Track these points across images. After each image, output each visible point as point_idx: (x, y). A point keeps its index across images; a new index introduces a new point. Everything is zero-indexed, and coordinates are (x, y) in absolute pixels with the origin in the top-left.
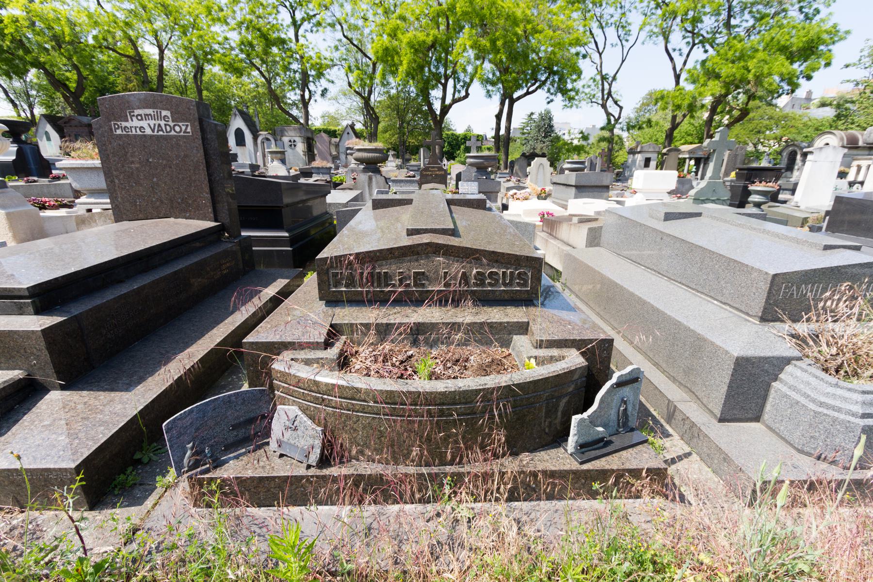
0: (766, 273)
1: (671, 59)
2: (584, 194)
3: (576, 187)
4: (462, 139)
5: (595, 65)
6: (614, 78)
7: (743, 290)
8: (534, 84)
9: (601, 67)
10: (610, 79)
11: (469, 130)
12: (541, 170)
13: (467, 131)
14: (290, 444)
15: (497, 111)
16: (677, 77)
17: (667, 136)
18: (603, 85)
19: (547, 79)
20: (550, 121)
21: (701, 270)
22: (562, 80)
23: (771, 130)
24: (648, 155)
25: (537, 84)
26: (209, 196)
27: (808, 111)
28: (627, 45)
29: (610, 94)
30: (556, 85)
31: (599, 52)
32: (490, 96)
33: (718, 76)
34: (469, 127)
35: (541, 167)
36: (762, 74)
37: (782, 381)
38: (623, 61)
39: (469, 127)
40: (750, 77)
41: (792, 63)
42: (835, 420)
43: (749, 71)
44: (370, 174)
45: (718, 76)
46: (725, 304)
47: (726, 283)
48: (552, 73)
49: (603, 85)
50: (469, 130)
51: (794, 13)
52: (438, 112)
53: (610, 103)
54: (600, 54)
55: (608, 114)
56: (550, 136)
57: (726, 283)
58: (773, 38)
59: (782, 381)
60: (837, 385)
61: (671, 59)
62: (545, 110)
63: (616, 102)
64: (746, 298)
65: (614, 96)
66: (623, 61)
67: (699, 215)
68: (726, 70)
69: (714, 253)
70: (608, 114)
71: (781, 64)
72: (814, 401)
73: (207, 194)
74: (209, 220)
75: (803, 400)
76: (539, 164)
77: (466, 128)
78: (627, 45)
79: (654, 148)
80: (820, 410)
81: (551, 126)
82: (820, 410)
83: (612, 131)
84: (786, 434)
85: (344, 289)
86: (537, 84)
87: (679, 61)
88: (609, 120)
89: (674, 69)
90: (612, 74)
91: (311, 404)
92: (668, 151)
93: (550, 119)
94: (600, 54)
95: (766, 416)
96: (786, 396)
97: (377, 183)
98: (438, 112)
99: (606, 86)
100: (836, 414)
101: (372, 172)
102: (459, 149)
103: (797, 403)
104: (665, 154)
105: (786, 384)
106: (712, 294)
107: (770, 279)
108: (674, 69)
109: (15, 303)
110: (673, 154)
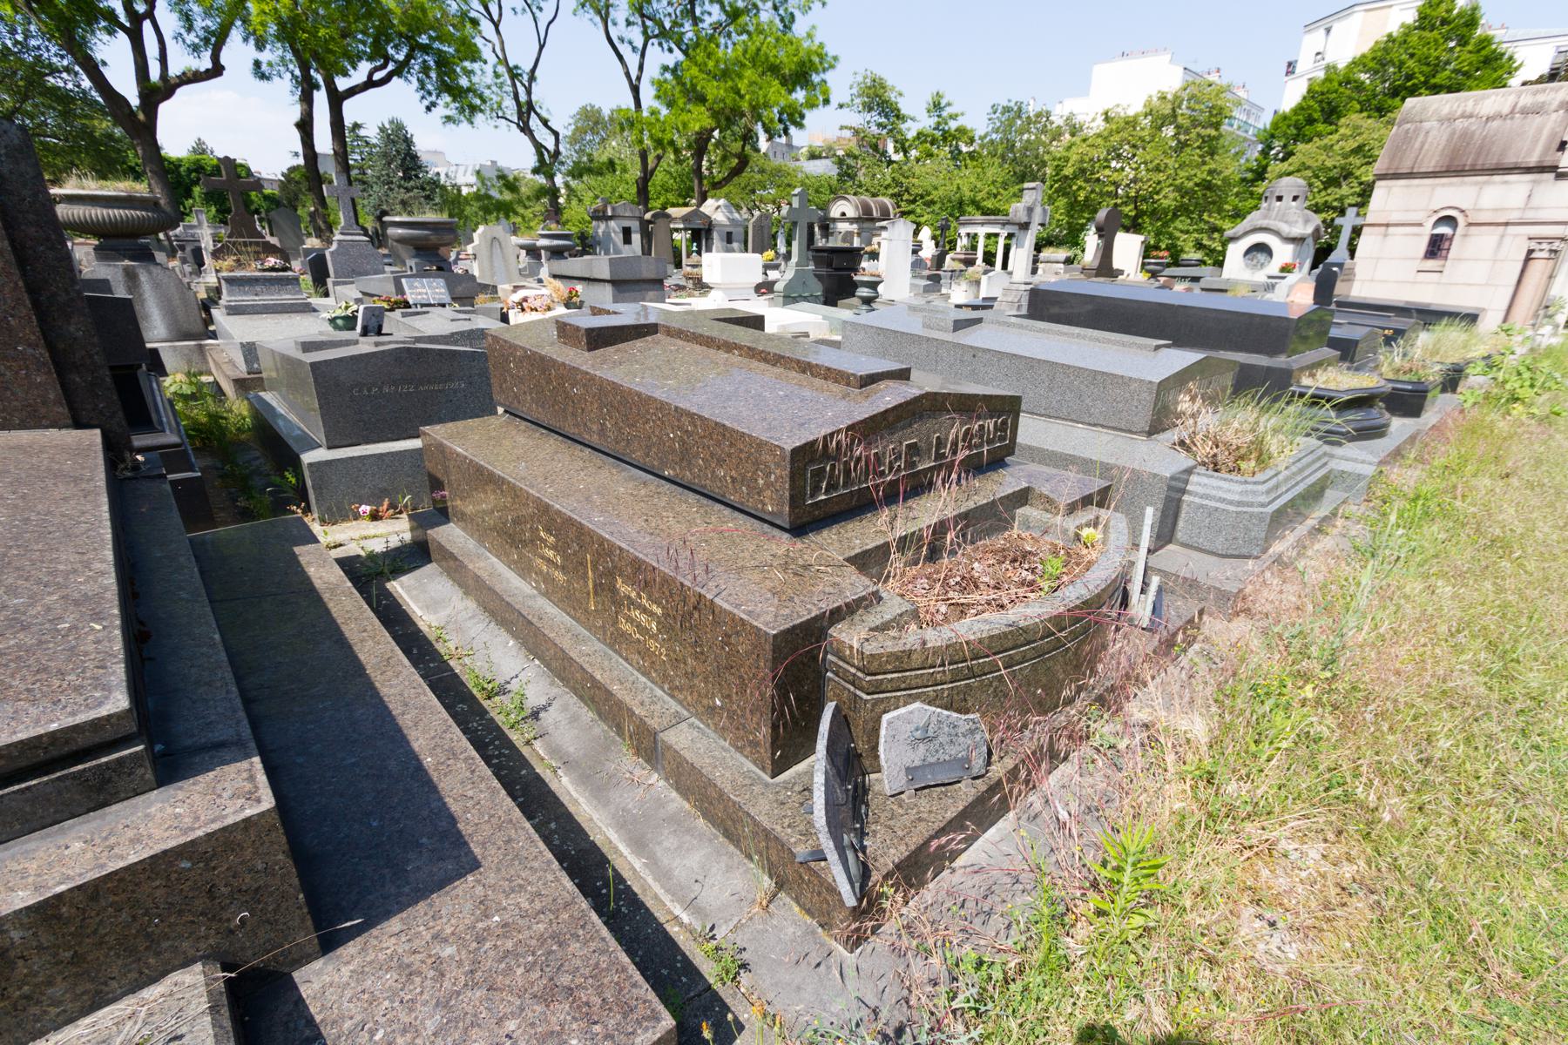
0: (1150, 382)
1: (620, 58)
2: (627, 295)
3: (613, 282)
4: (189, 171)
5: (490, 45)
6: (532, 78)
7: (1120, 405)
8: (384, 67)
9: (503, 50)
10: (526, 77)
11: (200, 148)
12: (497, 250)
13: (194, 151)
14: (931, 764)
15: (296, 113)
16: (635, 90)
17: (639, 192)
18: (514, 85)
19: (409, 57)
20: (409, 146)
21: (1051, 390)
22: (443, 63)
23: (764, 188)
24: (627, 223)
25: (391, 67)
26: (42, 353)
27: (798, 163)
28: (543, 19)
29: (531, 106)
30: (433, 75)
31: (492, 20)
32: (263, 77)
33: (702, 99)
34: (200, 142)
35: (496, 244)
36: (758, 104)
37: (1190, 493)
38: (542, 47)
39: (200, 142)
40: (745, 106)
41: (790, 92)
42: (1252, 515)
43: (742, 97)
44: (127, 262)
45: (702, 99)
46: (1095, 425)
47: (1093, 400)
48: (415, 48)
49: (514, 85)
50: (200, 148)
51: (766, 15)
52: (134, 101)
53: (534, 122)
54: (496, 25)
55: (539, 147)
56: (417, 176)
57: (1093, 400)
58: (759, 50)
59: (1190, 493)
60: (1246, 482)
61: (620, 58)
62: (391, 122)
63: (545, 123)
64: (1125, 413)
65: (538, 110)
66: (542, 47)
67: (979, 321)
68: (715, 91)
69: (1069, 367)
70: (539, 147)
71: (774, 89)
72: (1231, 503)
73: (34, 346)
74: (55, 424)
75: (1218, 505)
76: (489, 238)
77: (192, 143)
78: (543, 19)
79: (631, 210)
80: (1240, 509)
81: (415, 157)
82: (1240, 509)
83: (551, 177)
84: (1207, 546)
85: (823, 497)
86: (391, 67)
87: (632, 60)
88: (540, 155)
89: (628, 75)
90: (526, 66)
91: (899, 694)
92: (653, 216)
93: (408, 142)
94: (496, 25)
95: (1179, 535)
96: (1202, 506)
97: (157, 286)
98: (134, 101)
99: (521, 90)
100: (1250, 509)
101: (132, 259)
102: (189, 194)
103: (1217, 509)
104: (649, 222)
105: (1196, 494)
106: (1074, 417)
107: (1155, 388)
108: (628, 75)
109: (74, 776)
110: (660, 221)
